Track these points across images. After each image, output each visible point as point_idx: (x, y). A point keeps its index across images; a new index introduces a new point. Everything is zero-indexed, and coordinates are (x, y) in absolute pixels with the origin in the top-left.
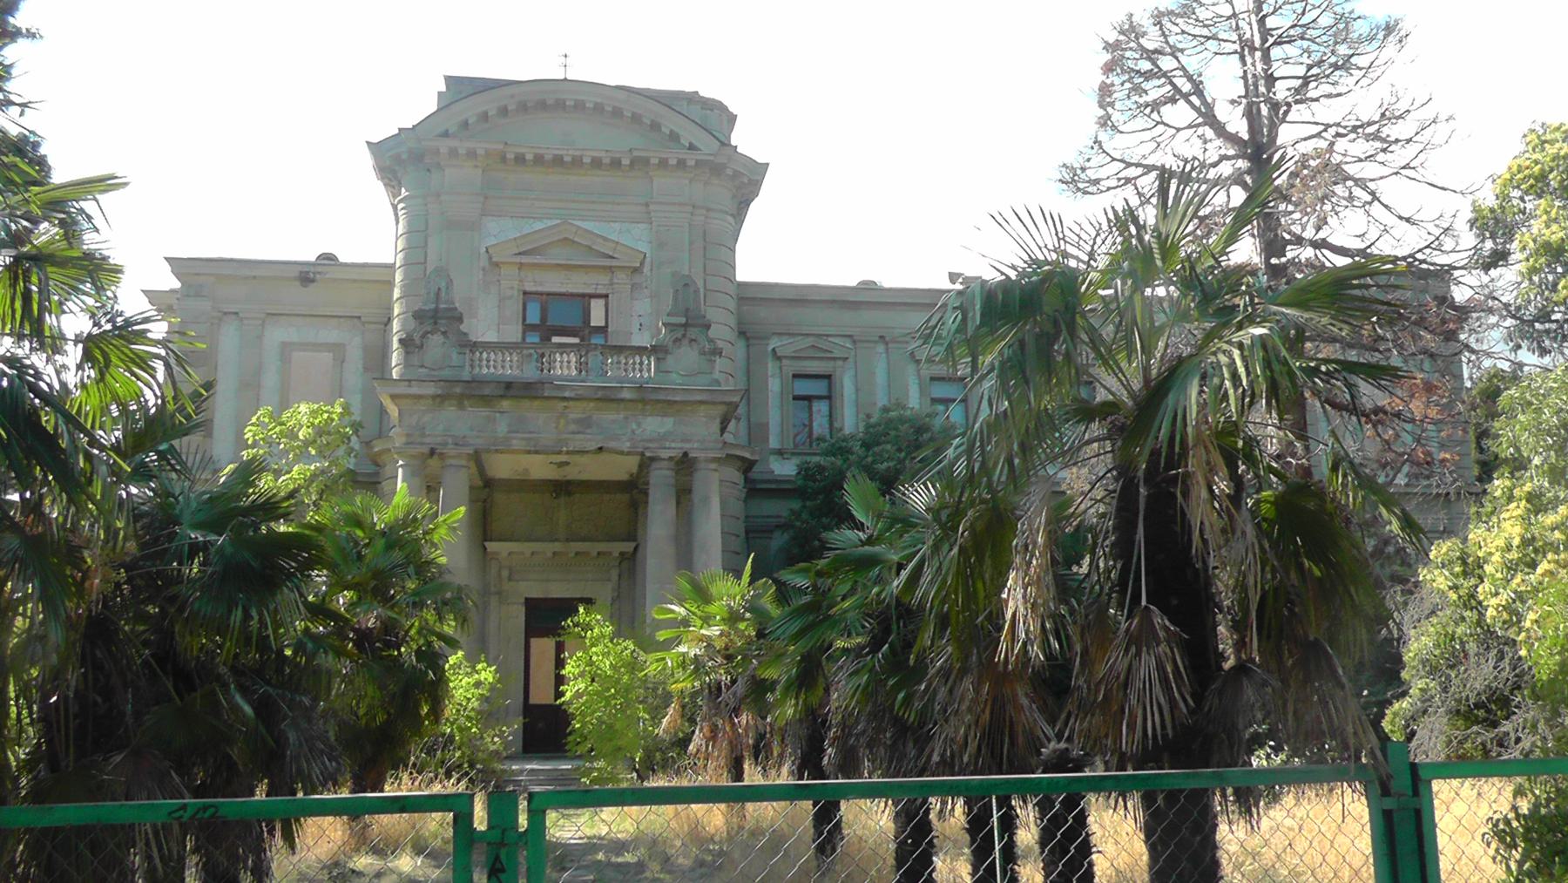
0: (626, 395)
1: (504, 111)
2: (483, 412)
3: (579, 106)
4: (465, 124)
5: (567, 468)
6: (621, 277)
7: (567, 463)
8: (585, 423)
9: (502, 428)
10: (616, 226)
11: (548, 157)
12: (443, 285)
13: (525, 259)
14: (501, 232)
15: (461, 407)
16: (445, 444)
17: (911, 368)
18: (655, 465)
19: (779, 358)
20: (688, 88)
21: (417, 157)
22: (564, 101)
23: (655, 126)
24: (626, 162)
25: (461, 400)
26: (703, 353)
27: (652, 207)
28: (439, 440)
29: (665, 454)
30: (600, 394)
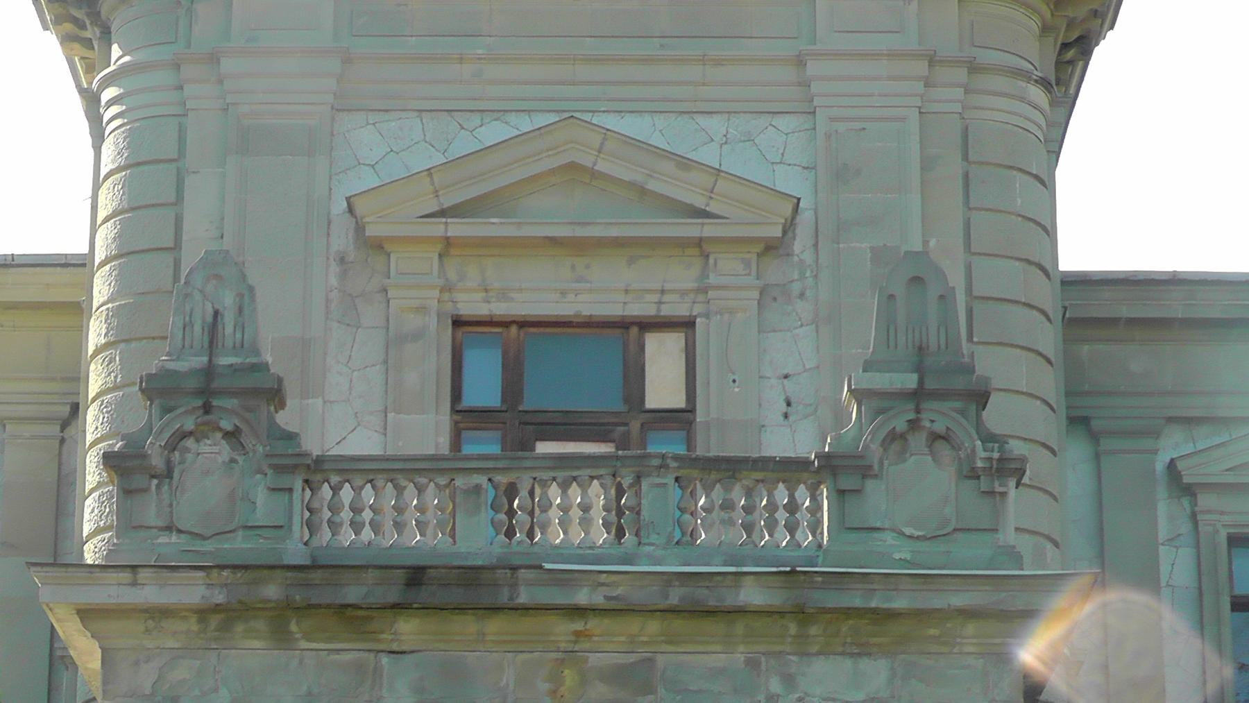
0: (752, 595)
2: (349, 653)
6: (728, 267)
10: (716, 125)
12: (228, 300)
13: (458, 228)
14: (387, 155)
15: (281, 637)
17: (1167, 514)
25: (281, 621)
27: (812, 68)
30: (675, 597)
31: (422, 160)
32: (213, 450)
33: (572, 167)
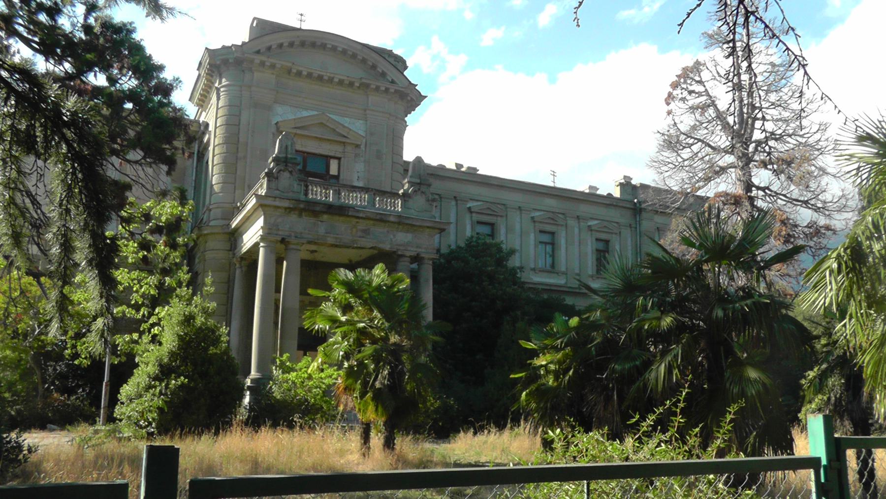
0: (392, 219)
1: (291, 45)
2: (312, 220)
3: (334, 49)
4: (269, 48)
5: (316, 254)
6: (349, 148)
7: (316, 251)
8: (366, 232)
9: (322, 230)
11: (315, 75)
12: (289, 143)
13: (299, 132)
14: (283, 114)
15: (300, 215)
16: (290, 236)
17: (468, 216)
18: (402, 259)
19: (471, 212)
20: (388, 46)
21: (238, 62)
22: (326, 44)
23: (374, 67)
24: (357, 84)
25: (301, 212)
26: (428, 200)
27: (368, 112)
28: (287, 233)
29: (408, 254)
30: (378, 217)
31: (291, 117)
32: (286, 174)
33: (322, 123)
